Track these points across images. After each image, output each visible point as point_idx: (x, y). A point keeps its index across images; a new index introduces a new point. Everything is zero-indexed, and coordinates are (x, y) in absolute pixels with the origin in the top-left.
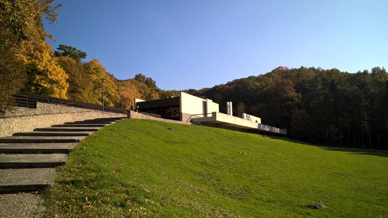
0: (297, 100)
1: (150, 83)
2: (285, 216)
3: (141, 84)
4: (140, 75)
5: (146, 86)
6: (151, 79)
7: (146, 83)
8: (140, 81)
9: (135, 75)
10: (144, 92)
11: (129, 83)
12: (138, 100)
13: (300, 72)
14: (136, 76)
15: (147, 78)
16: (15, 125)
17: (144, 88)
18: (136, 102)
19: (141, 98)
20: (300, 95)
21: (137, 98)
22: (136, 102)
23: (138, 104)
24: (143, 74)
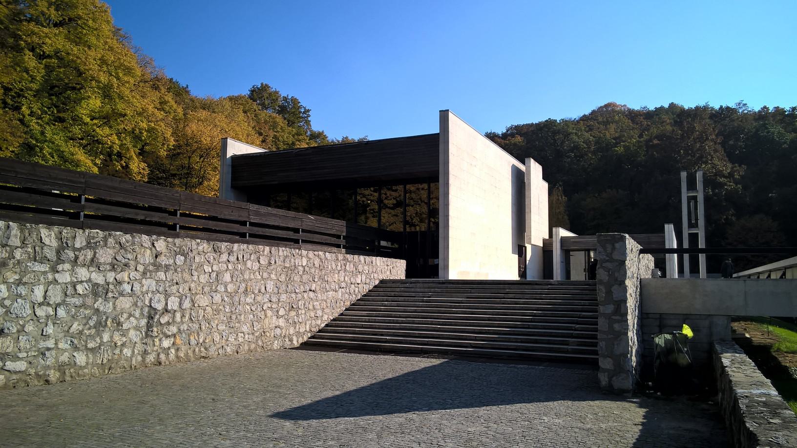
0: (731, 186)
1: (292, 112)
2: (702, 258)
3: (264, 114)
4: (265, 87)
5: (279, 119)
6: (295, 101)
7: (282, 110)
8: (264, 107)
9: (250, 87)
10: (275, 137)
11: (228, 105)
12: (237, 148)
13: (726, 113)
14: (252, 91)
15: (285, 99)
16: (45, 303)
17: (274, 126)
18: (230, 153)
19: (260, 146)
20: (741, 171)
21: (237, 138)
22: (230, 153)
23: (239, 161)
24: (274, 86)
